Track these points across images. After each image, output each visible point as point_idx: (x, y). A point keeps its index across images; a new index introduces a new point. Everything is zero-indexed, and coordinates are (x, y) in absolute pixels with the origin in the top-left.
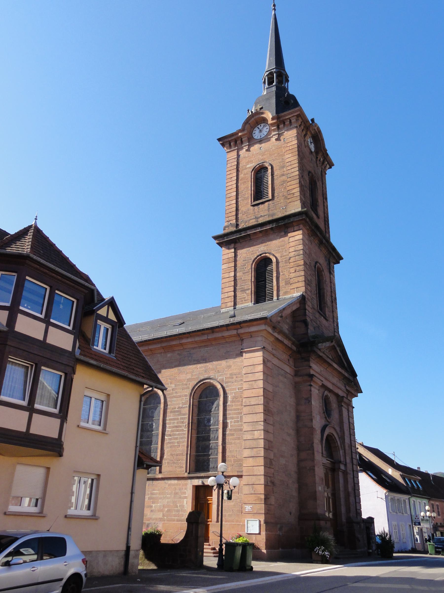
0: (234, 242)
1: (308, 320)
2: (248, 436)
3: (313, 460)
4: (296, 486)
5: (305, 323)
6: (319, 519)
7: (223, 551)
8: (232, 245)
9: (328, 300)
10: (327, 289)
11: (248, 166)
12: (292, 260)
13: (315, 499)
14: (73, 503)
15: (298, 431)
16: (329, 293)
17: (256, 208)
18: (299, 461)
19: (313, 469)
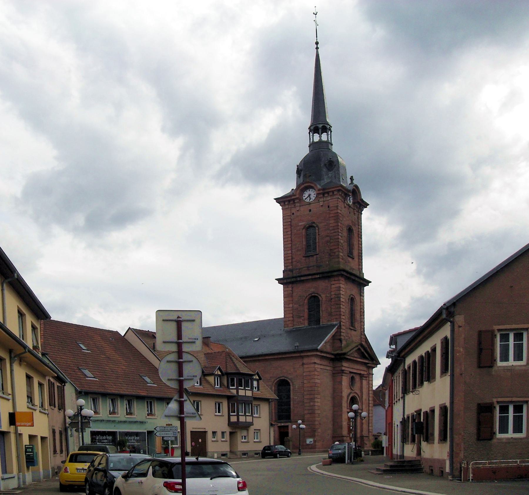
0: (292, 283)
1: (342, 337)
2: (308, 405)
3: (342, 411)
4: (332, 423)
5: (340, 340)
6: (343, 437)
7: (423, 429)
8: (290, 286)
9: (358, 316)
10: (357, 308)
11: (300, 224)
12: (333, 300)
13: (342, 428)
14: (383, 447)
15: (334, 398)
16: (359, 308)
17: (307, 259)
18: (334, 412)
19: (341, 415)
